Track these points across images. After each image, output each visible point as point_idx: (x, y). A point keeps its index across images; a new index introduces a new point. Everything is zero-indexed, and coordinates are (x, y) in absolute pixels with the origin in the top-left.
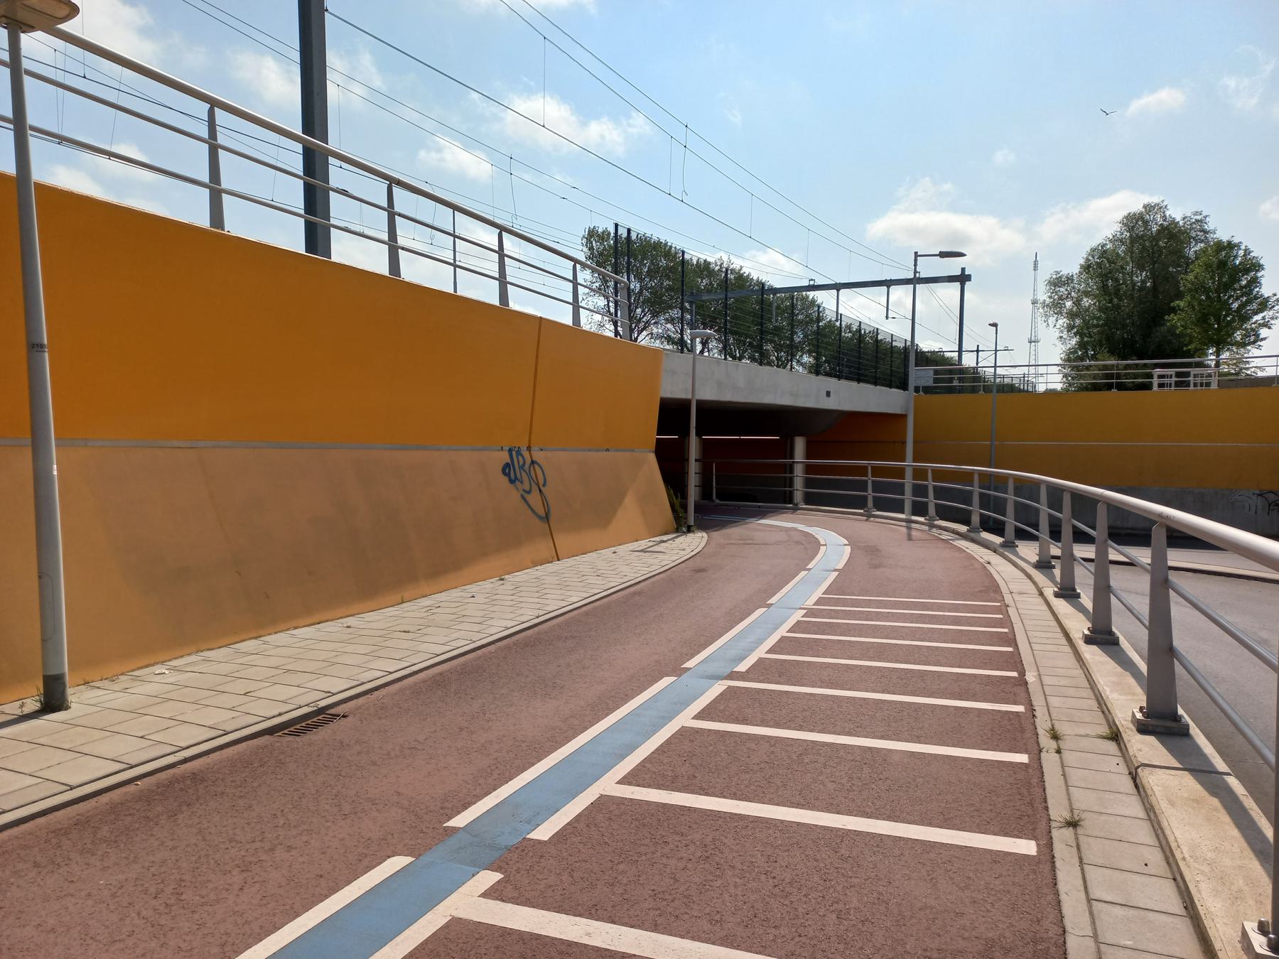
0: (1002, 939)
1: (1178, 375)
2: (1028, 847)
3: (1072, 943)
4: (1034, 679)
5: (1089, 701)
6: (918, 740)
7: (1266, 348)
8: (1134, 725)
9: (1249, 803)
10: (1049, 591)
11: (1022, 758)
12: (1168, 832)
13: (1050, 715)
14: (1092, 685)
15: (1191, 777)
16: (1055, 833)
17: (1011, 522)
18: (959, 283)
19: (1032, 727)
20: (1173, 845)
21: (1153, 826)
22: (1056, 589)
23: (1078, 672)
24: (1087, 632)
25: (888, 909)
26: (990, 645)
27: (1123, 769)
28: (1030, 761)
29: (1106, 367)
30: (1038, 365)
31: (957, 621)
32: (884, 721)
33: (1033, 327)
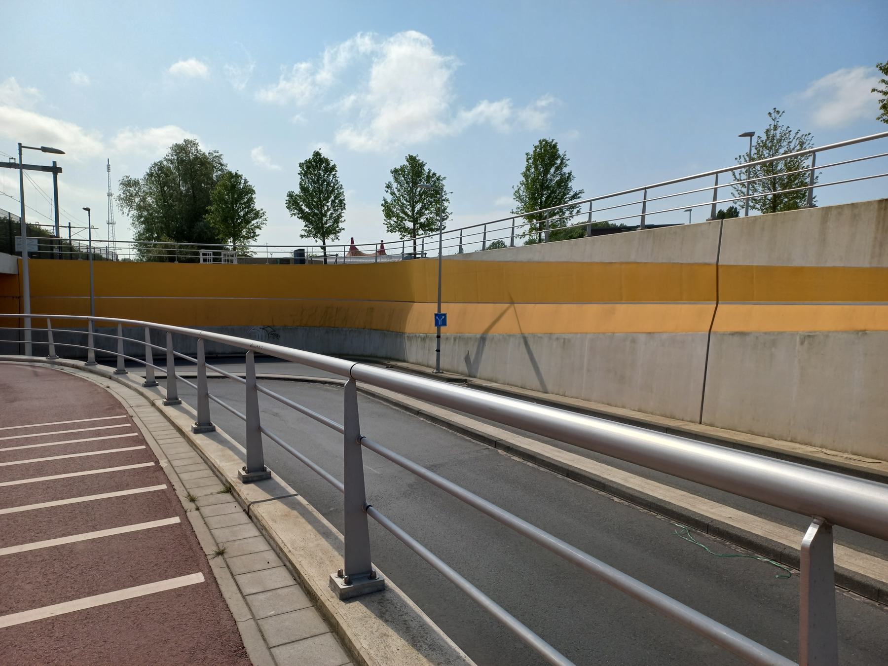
0: (199, 645)
2: (197, 578)
3: (241, 627)
4: (166, 465)
5: (206, 471)
6: (94, 528)
7: (260, 241)
8: (240, 480)
9: (311, 508)
10: (160, 403)
11: (176, 520)
12: (277, 539)
13: (184, 487)
14: (206, 460)
15: (279, 502)
16: (211, 563)
17: (121, 355)
19: (175, 497)
20: (282, 545)
21: (265, 538)
22: (165, 400)
23: (193, 454)
24: (195, 426)
25: (110, 661)
26: (128, 447)
27: (239, 509)
28: (181, 520)
29: (166, 246)
31: (98, 433)
32: (60, 523)
33: (110, 213)
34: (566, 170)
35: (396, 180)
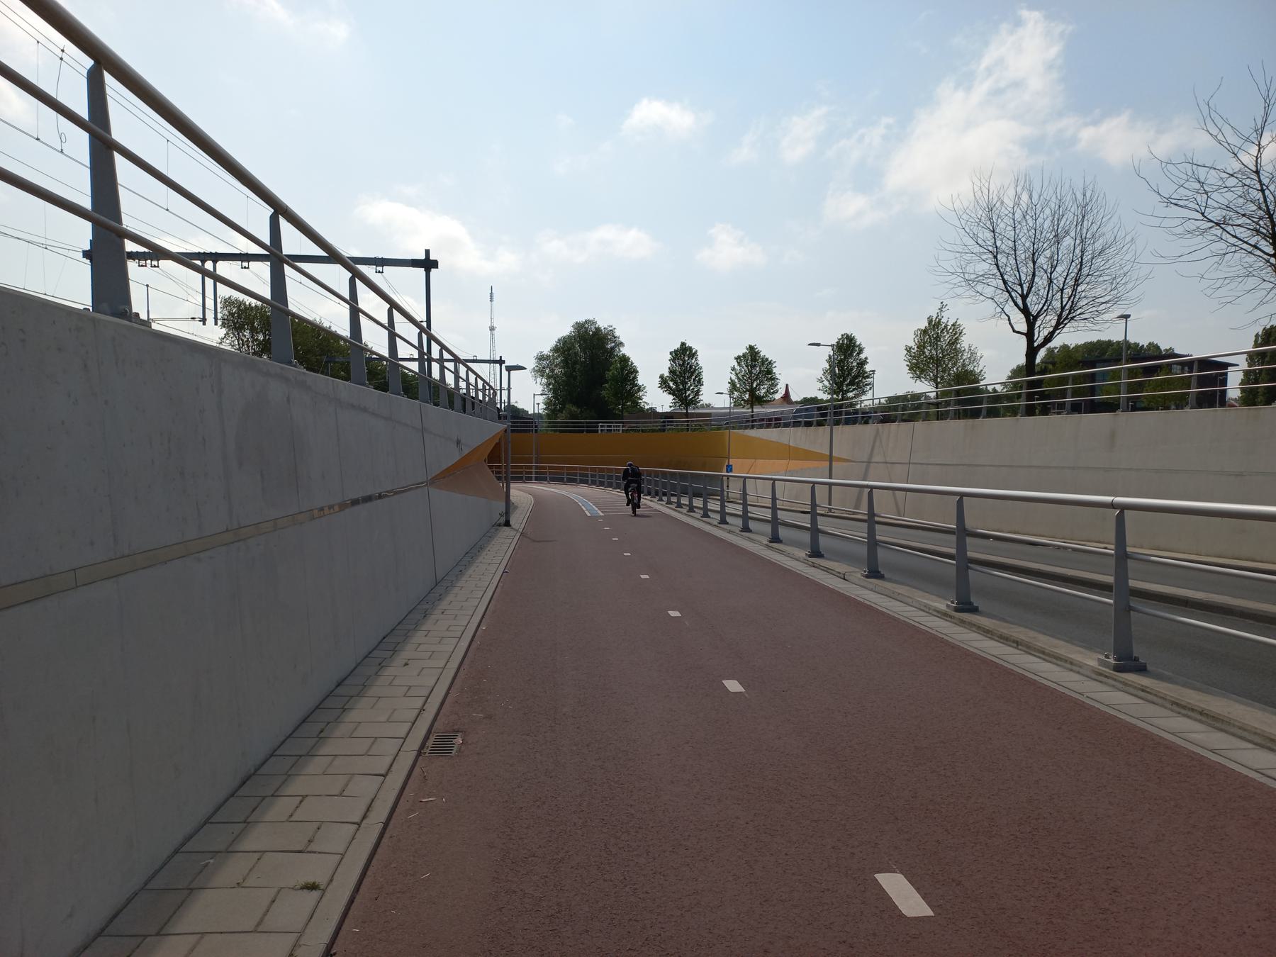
1: (608, 426)
18: (423, 269)
34: (863, 356)
35: (739, 364)
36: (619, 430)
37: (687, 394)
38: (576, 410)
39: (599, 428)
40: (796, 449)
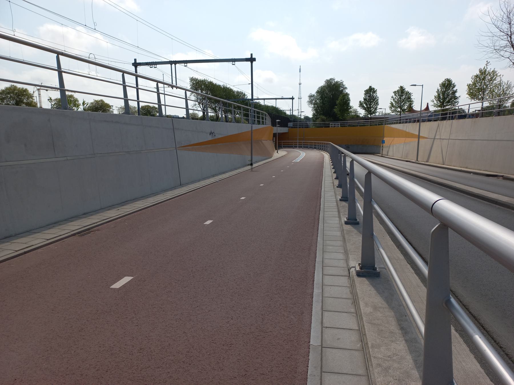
1: (334, 124)
18: (250, 62)
30: (164, 88)
34: (455, 89)
35: (395, 95)
36: (338, 126)
37: (371, 109)
38: (324, 117)
39: (330, 125)
40: (409, 133)
